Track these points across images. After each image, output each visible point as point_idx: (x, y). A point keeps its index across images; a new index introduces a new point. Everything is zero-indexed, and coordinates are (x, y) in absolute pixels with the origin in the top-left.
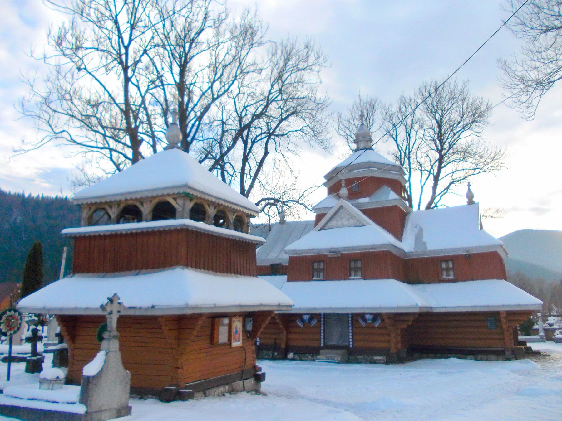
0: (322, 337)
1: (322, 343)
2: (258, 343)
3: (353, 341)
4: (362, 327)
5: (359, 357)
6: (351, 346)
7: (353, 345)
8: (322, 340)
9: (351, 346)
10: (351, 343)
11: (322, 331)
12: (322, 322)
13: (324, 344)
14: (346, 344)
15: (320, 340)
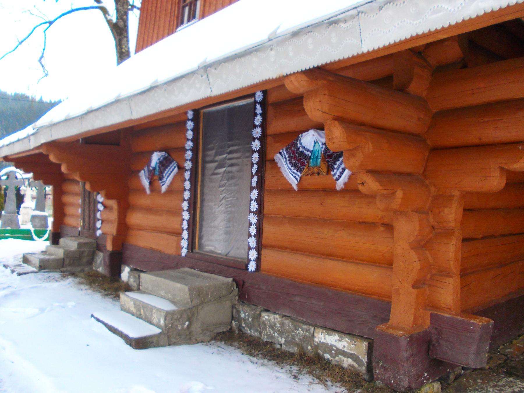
0: (185, 225)
1: (184, 244)
2: (99, 233)
3: (259, 248)
4: (289, 190)
5: (265, 316)
6: (252, 266)
7: (258, 261)
8: (185, 235)
9: (252, 266)
10: (253, 254)
11: (185, 205)
12: (187, 175)
13: (191, 246)
14: (237, 253)
15: (178, 234)
